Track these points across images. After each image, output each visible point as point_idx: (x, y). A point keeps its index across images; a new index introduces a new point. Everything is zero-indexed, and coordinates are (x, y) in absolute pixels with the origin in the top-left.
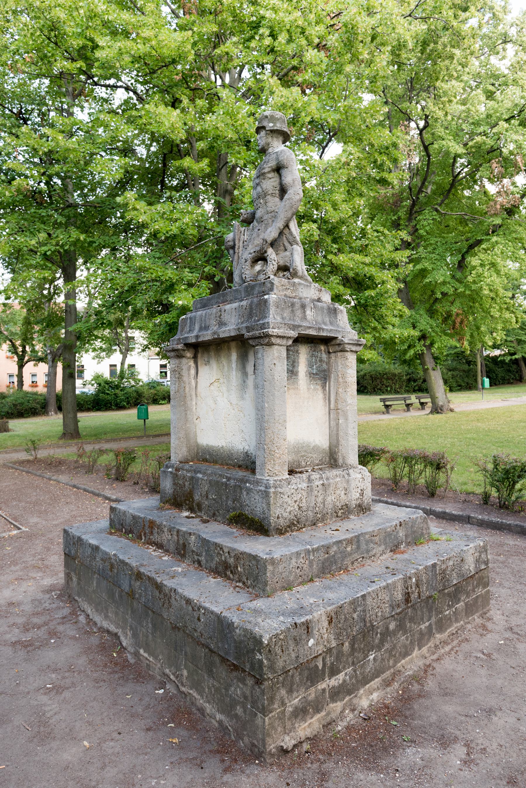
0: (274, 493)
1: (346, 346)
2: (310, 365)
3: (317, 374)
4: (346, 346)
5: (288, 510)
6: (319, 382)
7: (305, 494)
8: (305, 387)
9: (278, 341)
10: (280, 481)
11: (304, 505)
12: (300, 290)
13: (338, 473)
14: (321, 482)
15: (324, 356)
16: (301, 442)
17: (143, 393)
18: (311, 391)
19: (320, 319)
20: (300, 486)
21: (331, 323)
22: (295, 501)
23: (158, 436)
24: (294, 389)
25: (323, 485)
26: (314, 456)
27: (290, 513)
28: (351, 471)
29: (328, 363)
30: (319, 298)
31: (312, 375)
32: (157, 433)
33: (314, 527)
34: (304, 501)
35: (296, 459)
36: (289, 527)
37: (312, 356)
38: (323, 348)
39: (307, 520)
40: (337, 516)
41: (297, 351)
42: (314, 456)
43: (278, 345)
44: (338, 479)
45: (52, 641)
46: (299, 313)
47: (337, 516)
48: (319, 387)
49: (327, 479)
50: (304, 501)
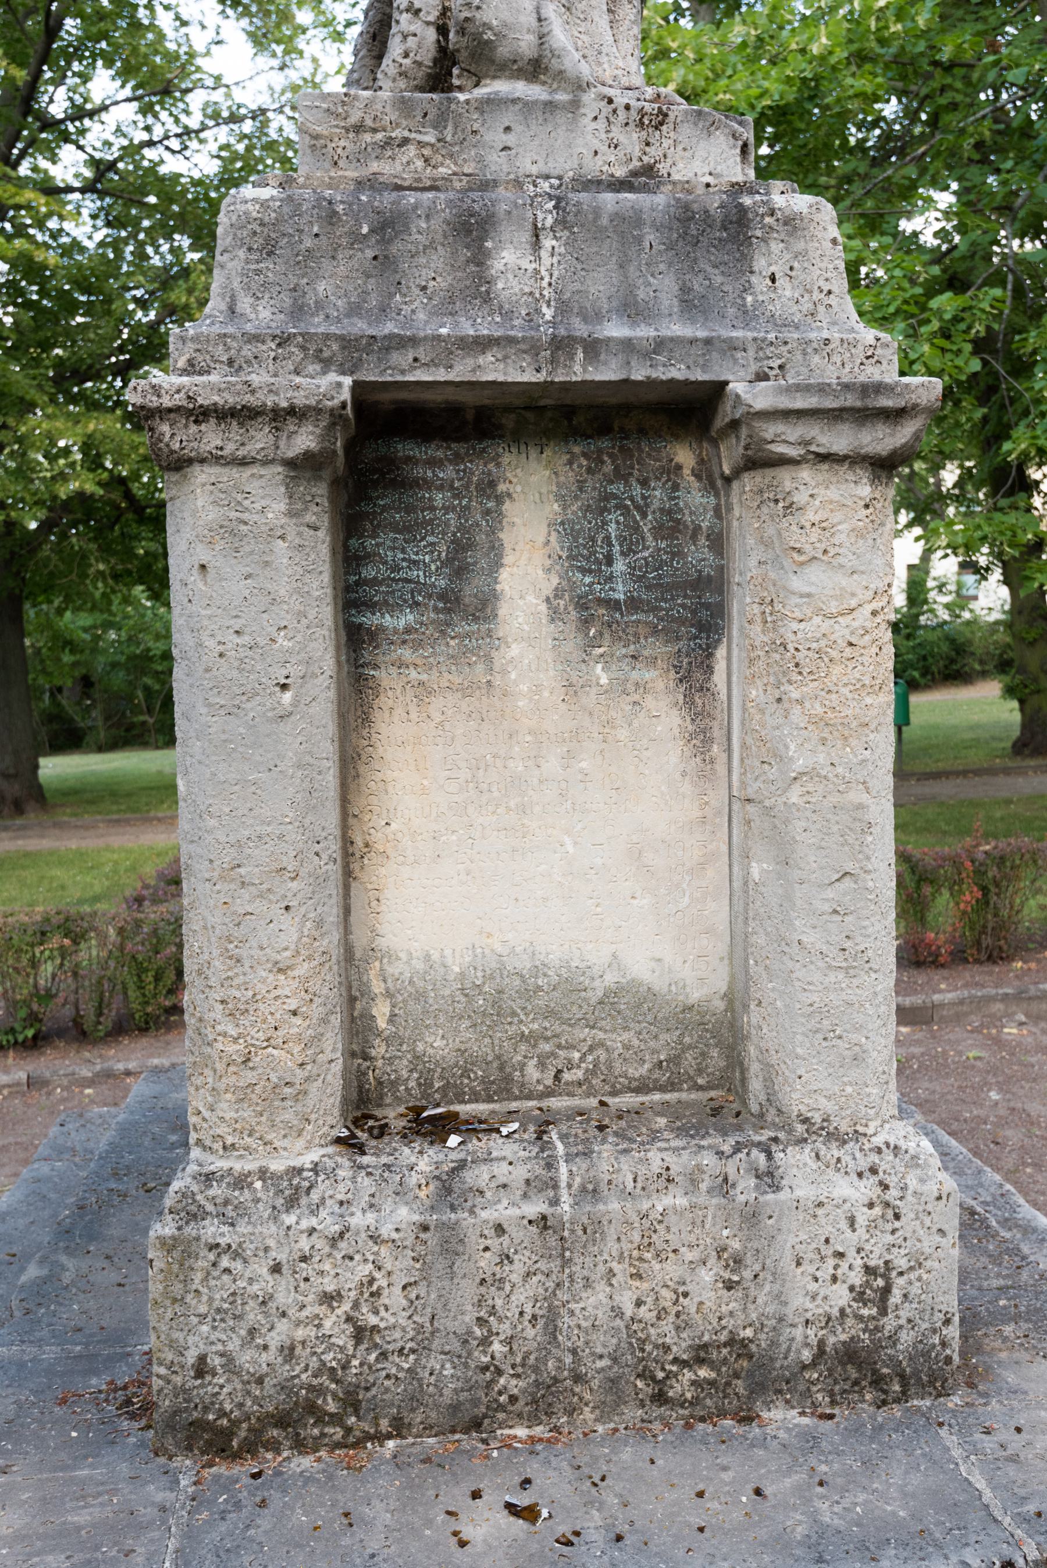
0: (168, 1245)
1: (770, 430)
2: (584, 553)
3: (633, 604)
4: (770, 430)
5: (275, 1339)
6: (656, 648)
7: (400, 1267)
8: (550, 677)
9: (212, 437)
10: (241, 1182)
11: (393, 1315)
12: (495, 137)
13: (678, 1164)
14: (534, 1208)
15: (695, 499)
16: (524, 964)
17: (970, 642)
18: (590, 698)
19: (600, 285)
20: (359, 1220)
21: (690, 304)
22: (329, 1299)
23: (936, 776)
24: (466, 691)
25: (543, 1222)
26: (617, 1041)
27: (289, 1352)
28: (795, 1161)
29: (718, 542)
30: (649, 170)
31: (593, 613)
32: (933, 767)
33: (469, 1442)
34: (394, 1298)
35: (483, 1049)
36: (282, 1420)
37: (601, 507)
38: (685, 456)
39: (415, 1400)
40: (660, 1398)
41: (488, 487)
42: (617, 1041)
43: (216, 459)
44: (675, 1199)
45: (74, 1434)
46: (434, 269)
47: (660, 1398)
48: (657, 681)
49: (590, 1192)
50: (394, 1298)
